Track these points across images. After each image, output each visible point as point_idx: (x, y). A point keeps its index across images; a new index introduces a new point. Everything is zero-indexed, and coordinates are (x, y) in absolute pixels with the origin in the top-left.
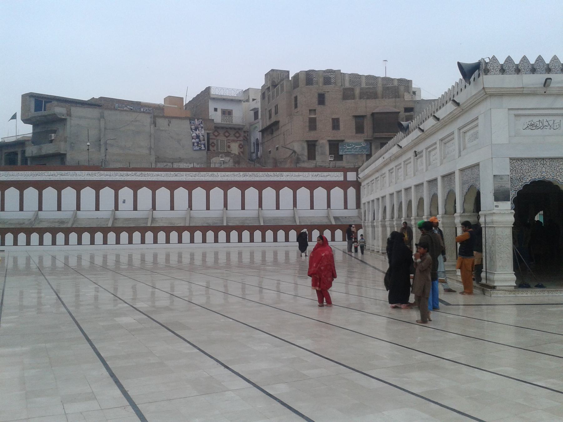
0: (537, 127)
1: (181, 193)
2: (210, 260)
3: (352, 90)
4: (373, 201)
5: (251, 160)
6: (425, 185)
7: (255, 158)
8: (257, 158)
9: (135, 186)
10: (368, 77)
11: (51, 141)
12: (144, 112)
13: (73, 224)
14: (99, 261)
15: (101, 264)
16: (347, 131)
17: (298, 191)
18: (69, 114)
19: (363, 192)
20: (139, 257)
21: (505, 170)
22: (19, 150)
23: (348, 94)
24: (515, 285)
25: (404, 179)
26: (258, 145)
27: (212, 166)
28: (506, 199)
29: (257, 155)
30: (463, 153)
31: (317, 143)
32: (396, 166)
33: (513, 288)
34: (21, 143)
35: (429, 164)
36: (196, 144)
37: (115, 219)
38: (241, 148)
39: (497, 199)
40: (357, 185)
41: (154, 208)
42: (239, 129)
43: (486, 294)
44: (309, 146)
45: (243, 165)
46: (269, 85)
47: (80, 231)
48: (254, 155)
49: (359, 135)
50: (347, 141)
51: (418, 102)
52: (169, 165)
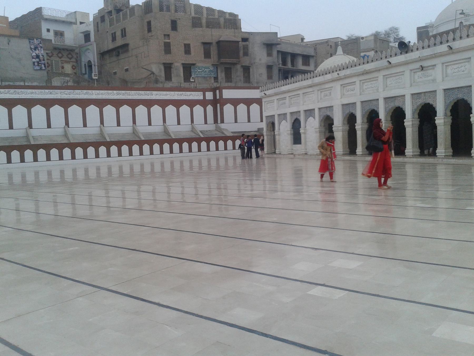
3: (199, 19)
16: (197, 55)
17: (69, 109)
31: (173, 66)
36: (36, 64)
38: (74, 69)
44: (165, 68)
47: (35, 148)
49: (207, 60)
50: (199, 65)
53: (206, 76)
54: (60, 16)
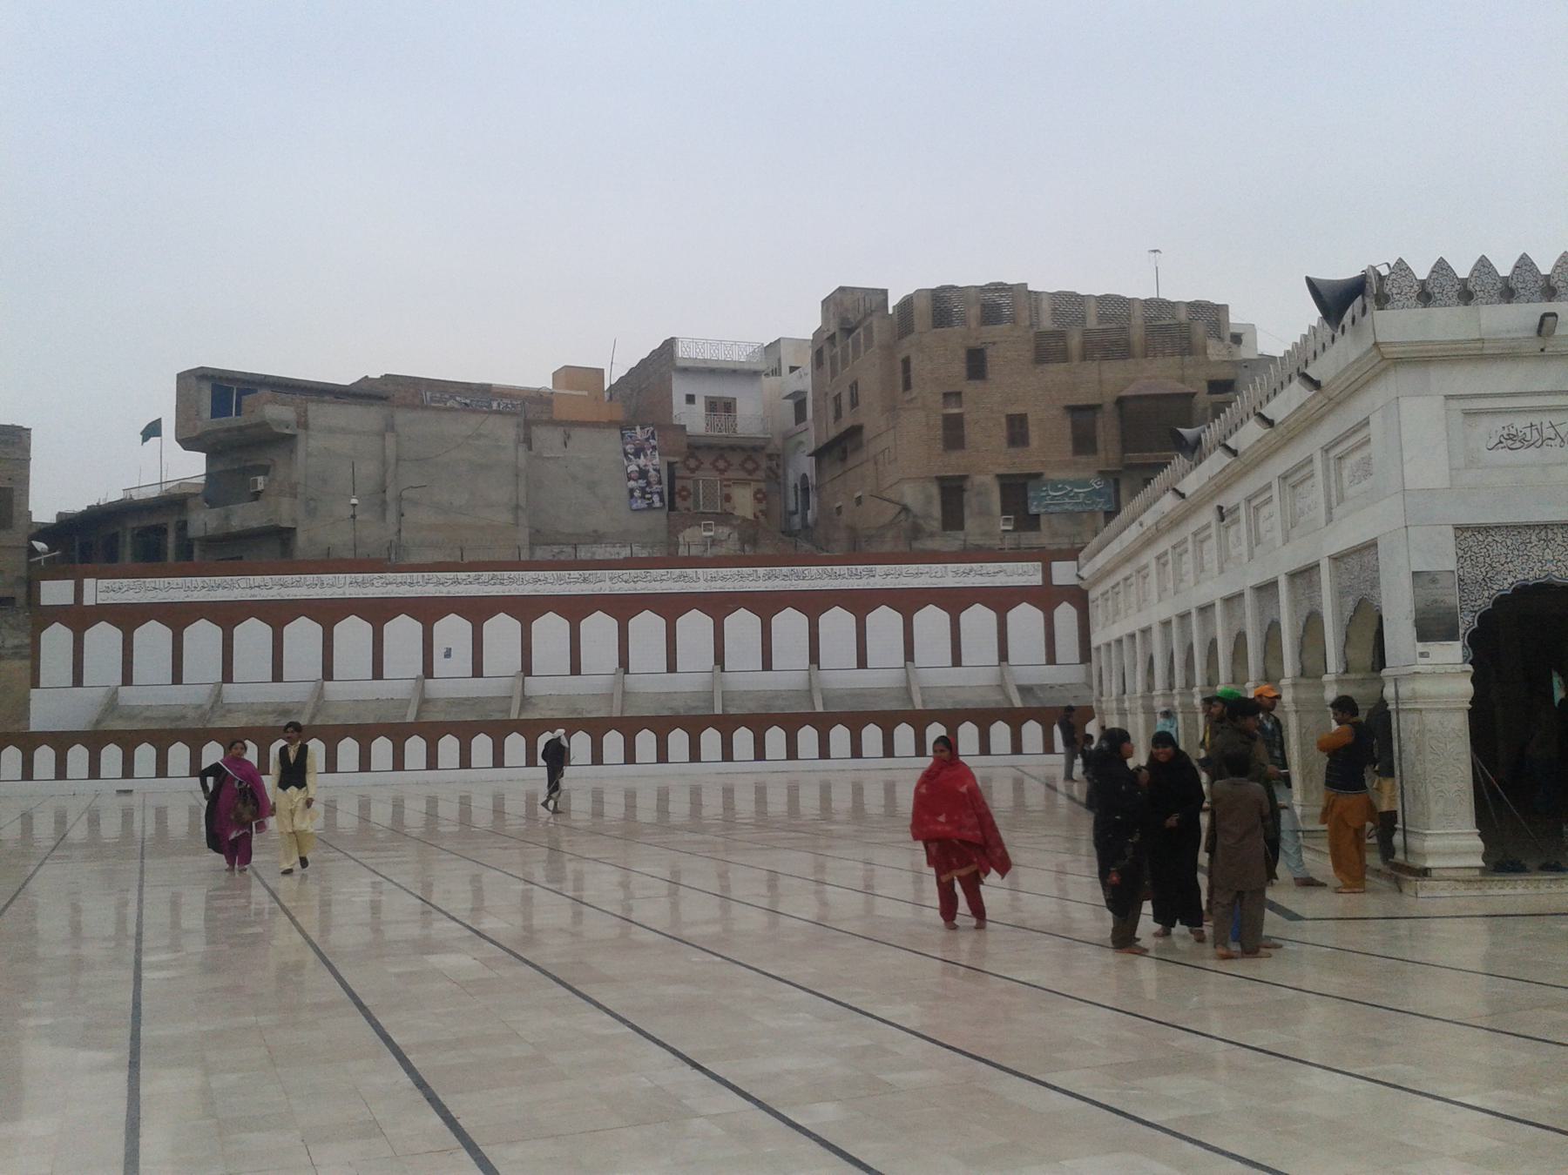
0: (1525, 443)
1: (599, 628)
2: (679, 807)
3: (1061, 335)
4: (1119, 641)
5: (788, 533)
6: (1249, 598)
7: (798, 527)
8: (805, 526)
9: (477, 611)
10: (1104, 300)
11: (257, 496)
12: (498, 412)
13: (313, 717)
14: (381, 814)
15: (387, 822)
16: (1049, 451)
18: (303, 424)
19: (1097, 615)
20: (488, 803)
21: (1443, 558)
22: (171, 523)
23: (1048, 349)
24: (1481, 864)
25: (1197, 583)
26: (806, 491)
27: (683, 551)
28: (1451, 635)
29: (804, 517)
30: (1337, 512)
31: (968, 485)
32: (1174, 547)
33: (1477, 872)
34: (174, 503)
35: (1256, 540)
37: (424, 701)
38: (759, 501)
39: (1424, 634)
40: (1079, 597)
41: (527, 669)
42: (755, 449)
43: (1405, 890)
45: (767, 550)
46: (833, 328)
48: (797, 519)
49: (1083, 459)
50: (1052, 475)
51: (1247, 364)
52: (567, 553)
53: (1077, 509)
54: (736, 358)
